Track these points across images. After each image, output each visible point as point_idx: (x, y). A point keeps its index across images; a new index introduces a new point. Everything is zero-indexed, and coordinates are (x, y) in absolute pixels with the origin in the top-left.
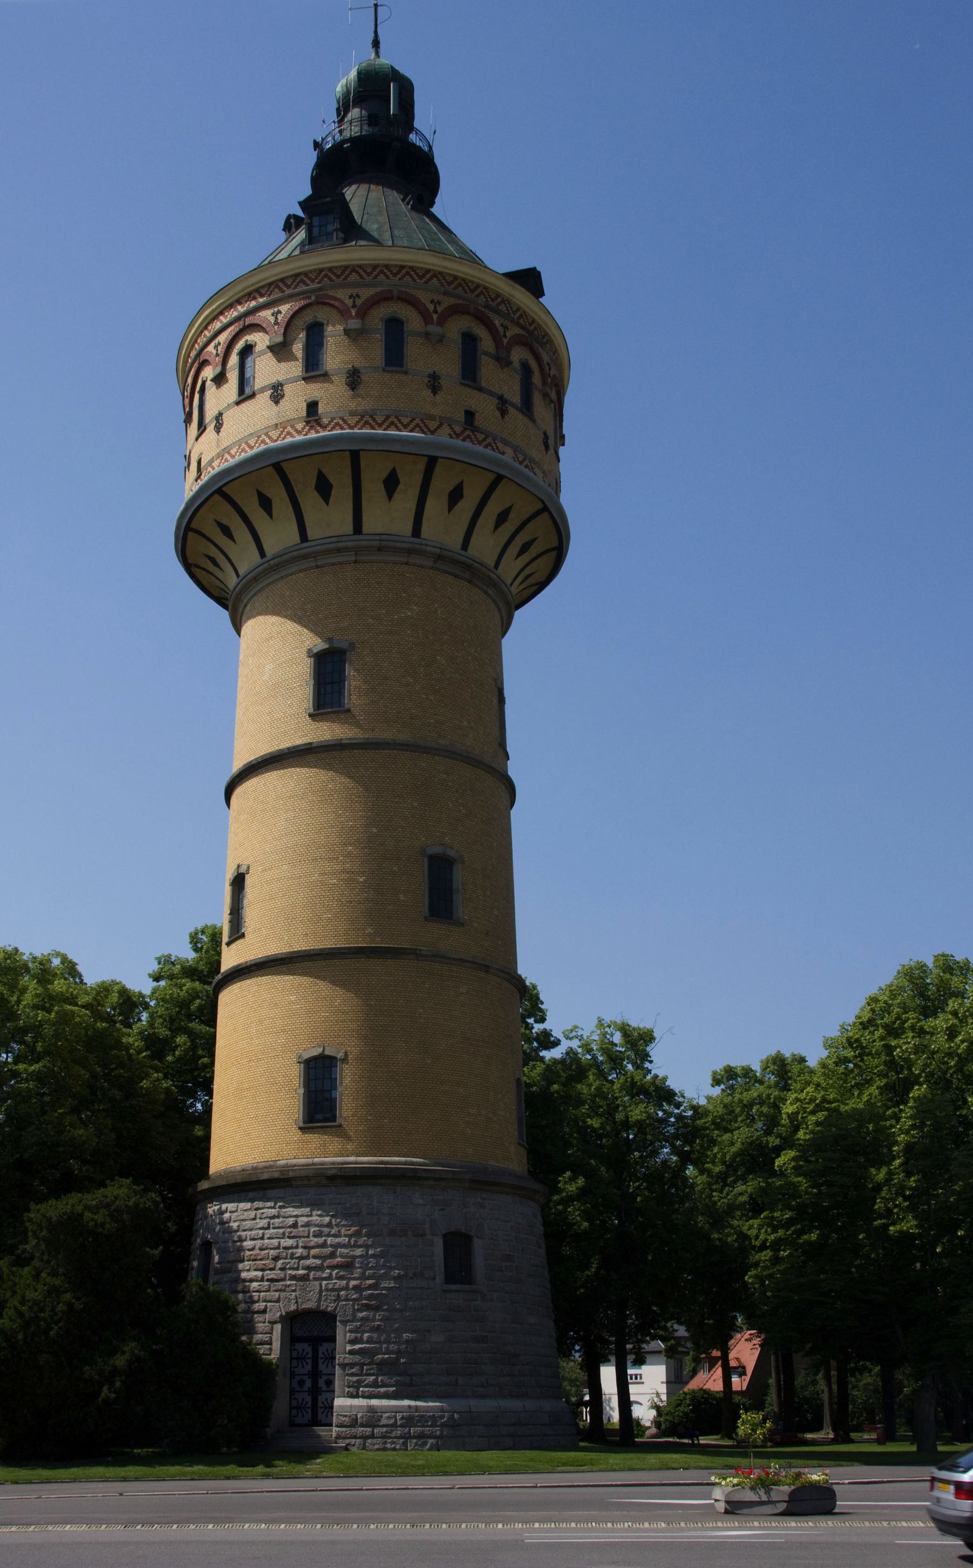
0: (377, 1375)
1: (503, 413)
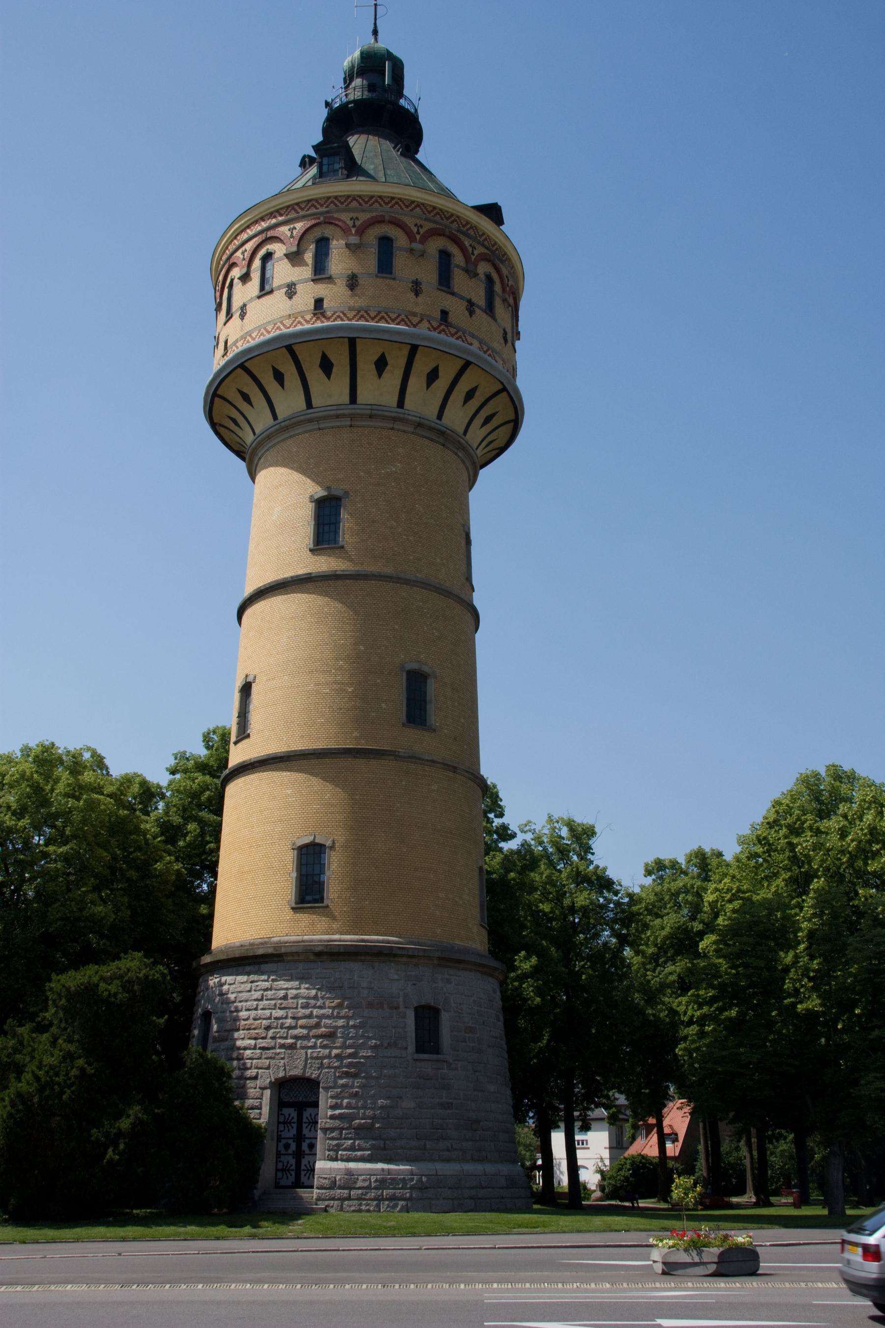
1: (471, 313)
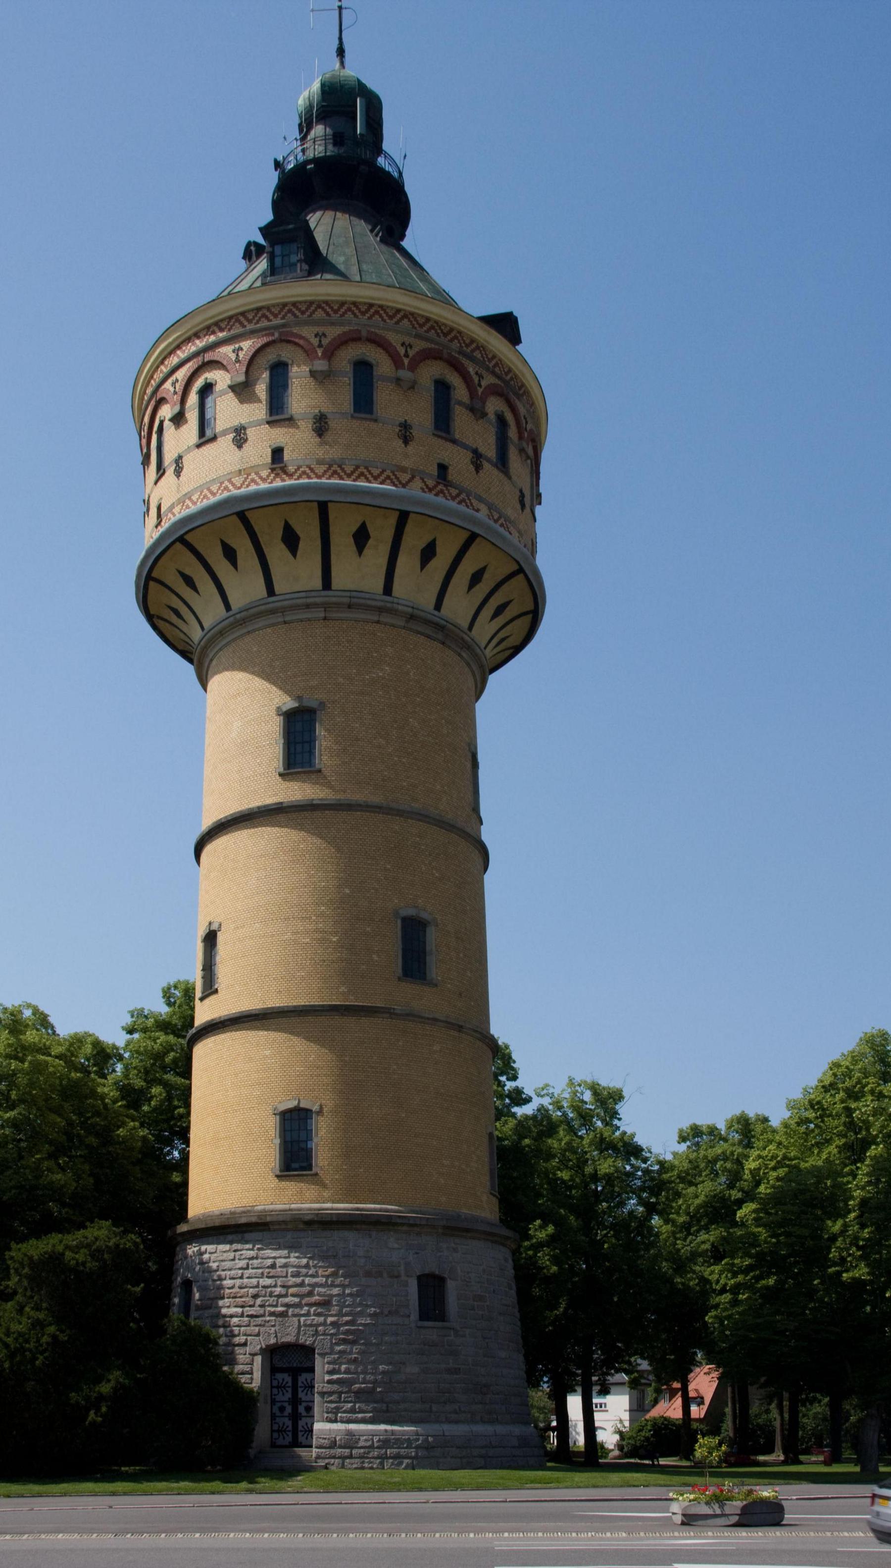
0: (355, 1403)
1: (478, 468)
